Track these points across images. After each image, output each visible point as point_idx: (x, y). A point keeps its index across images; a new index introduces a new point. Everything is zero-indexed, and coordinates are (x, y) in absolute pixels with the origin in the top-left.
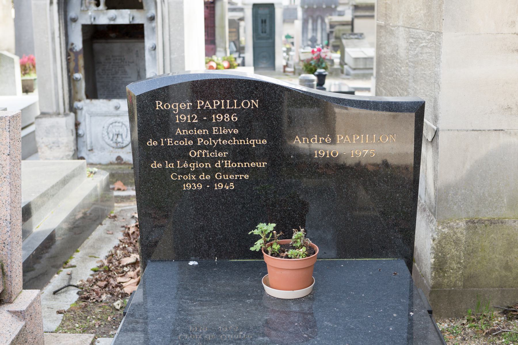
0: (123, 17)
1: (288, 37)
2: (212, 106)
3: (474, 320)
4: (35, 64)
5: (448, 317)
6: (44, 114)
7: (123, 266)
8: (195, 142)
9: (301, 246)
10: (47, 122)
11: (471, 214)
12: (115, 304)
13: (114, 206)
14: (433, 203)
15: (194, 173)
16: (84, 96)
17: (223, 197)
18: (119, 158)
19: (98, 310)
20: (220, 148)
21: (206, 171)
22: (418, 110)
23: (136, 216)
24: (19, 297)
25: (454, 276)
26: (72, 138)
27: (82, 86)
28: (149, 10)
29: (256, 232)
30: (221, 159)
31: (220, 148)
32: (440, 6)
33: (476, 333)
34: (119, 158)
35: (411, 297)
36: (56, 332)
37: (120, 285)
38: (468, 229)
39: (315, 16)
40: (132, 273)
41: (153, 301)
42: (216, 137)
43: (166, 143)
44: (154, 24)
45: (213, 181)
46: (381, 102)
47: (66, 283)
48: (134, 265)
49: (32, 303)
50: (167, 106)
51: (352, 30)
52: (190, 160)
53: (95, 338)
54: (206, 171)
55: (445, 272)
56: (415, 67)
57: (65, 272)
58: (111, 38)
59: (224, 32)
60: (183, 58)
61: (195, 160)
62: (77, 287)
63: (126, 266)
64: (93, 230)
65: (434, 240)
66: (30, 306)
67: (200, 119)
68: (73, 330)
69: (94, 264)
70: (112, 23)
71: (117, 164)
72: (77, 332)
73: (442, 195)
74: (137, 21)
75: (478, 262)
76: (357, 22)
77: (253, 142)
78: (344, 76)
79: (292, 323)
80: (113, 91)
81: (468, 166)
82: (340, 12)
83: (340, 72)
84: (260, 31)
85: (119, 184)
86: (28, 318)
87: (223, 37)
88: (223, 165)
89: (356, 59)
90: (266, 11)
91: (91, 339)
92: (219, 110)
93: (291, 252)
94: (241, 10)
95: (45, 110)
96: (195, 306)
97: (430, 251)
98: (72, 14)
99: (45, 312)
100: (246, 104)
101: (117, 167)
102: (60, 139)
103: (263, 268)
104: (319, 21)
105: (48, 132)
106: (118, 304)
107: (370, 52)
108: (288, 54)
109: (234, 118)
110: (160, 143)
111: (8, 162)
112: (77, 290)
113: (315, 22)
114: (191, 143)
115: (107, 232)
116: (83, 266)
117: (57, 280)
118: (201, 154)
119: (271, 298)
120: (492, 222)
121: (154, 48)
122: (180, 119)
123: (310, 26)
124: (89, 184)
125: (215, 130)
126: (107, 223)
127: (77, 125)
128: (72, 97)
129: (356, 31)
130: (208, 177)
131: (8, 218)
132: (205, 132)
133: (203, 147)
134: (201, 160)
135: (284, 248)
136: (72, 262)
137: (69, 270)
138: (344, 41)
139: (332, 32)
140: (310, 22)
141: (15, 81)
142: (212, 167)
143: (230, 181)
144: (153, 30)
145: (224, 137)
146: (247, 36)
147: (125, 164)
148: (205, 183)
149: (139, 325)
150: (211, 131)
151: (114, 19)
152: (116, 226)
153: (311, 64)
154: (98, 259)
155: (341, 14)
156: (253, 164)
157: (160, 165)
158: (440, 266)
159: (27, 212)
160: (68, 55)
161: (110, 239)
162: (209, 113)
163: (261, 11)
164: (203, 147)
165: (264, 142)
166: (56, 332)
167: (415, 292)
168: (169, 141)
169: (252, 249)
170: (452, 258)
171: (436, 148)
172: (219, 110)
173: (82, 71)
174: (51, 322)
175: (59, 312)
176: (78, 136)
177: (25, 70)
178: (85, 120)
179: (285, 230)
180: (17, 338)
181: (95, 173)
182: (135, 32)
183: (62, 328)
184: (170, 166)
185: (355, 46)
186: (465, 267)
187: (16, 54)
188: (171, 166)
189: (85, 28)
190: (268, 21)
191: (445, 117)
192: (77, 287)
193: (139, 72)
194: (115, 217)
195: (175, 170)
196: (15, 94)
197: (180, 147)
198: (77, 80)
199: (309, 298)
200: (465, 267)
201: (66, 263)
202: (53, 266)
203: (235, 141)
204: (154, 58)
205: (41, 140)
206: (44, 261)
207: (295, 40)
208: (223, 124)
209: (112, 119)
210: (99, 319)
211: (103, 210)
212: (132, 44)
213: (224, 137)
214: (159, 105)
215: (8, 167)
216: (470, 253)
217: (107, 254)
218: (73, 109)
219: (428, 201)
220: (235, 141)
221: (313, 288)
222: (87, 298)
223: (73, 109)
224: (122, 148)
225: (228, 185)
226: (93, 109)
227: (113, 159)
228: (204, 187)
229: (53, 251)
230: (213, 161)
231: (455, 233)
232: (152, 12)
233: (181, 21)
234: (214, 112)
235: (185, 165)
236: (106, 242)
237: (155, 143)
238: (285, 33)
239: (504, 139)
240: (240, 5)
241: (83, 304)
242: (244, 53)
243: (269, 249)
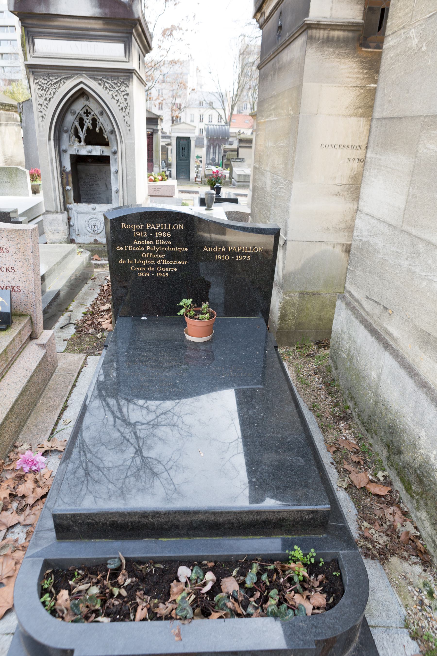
0: (96, 151)
1: (198, 157)
2: (156, 227)
3: (300, 348)
4: (40, 174)
5: (286, 346)
6: (48, 212)
7: (101, 312)
8: (145, 248)
9: (207, 313)
10: (50, 217)
11: (302, 289)
12: (98, 336)
13: (93, 272)
14: (282, 282)
15: (144, 267)
16: (73, 201)
17: (162, 281)
18: (95, 240)
19: (88, 339)
20: (160, 252)
21: (152, 266)
22: (276, 233)
23: (109, 278)
24: (42, 335)
25: (290, 323)
26: (67, 227)
27: (71, 194)
28: (113, 147)
29: (181, 304)
30: (161, 259)
31: (160, 252)
32: (293, 165)
33: (300, 355)
34: (95, 240)
35: (266, 342)
36: (63, 352)
37: (100, 324)
38: (300, 297)
39: (215, 144)
40: (106, 316)
41: (122, 342)
42: (158, 246)
43: (128, 248)
44: (116, 157)
45: (156, 271)
46: (255, 228)
47: (67, 322)
48: (108, 311)
49: (50, 339)
50: (129, 227)
51: (238, 156)
52: (142, 259)
53: (87, 356)
54: (152, 266)
55: (286, 321)
56: (275, 199)
57: (67, 314)
58: (88, 162)
59: (158, 154)
60: (135, 179)
61: (145, 259)
62: (74, 324)
63: (103, 311)
64: (82, 288)
65: (280, 303)
66: (48, 341)
67: (148, 234)
68: (73, 351)
69: (84, 310)
70: (89, 154)
71: (95, 244)
72: (76, 353)
73: (286, 278)
74: (106, 154)
75: (305, 316)
76: (240, 150)
77: (180, 249)
78: (231, 186)
79: (201, 357)
80: (91, 196)
81: (302, 262)
82: (230, 142)
83: (229, 184)
84: (181, 155)
85: (96, 257)
86: (48, 347)
87: (158, 157)
88: (162, 262)
89: (239, 175)
90: (185, 142)
91: (85, 357)
92: (160, 230)
93: (201, 316)
94: (169, 137)
95: (49, 209)
96: (146, 346)
97: (278, 309)
98: (63, 147)
99: (57, 340)
100: (176, 227)
101: (94, 245)
102: (59, 228)
103: (185, 325)
104: (217, 147)
105: (51, 224)
106: (99, 336)
107: (248, 171)
108: (197, 169)
109: (169, 235)
110: (124, 248)
111: (31, 257)
112: (75, 326)
113: (214, 147)
114: (143, 249)
115: (91, 288)
116: (77, 311)
117: (62, 320)
118: (149, 256)
119: (189, 341)
120: (313, 294)
121: (117, 172)
122: (136, 235)
123: (212, 150)
124: (79, 260)
125: (157, 241)
126: (90, 282)
127: (69, 219)
128: (66, 201)
129: (240, 157)
130: (153, 269)
131: (33, 290)
132: (151, 242)
133: (150, 252)
134: (149, 259)
135: (198, 313)
136: (71, 308)
137: (68, 314)
138: (232, 163)
139: (225, 155)
140: (212, 147)
141: (27, 186)
142: (155, 260)
143: (166, 272)
144: (116, 160)
145: (162, 246)
146: (173, 158)
147: (100, 244)
148: (151, 272)
149: (114, 357)
150: (155, 242)
151: (91, 152)
152: (96, 285)
153: (212, 180)
154: (86, 307)
155: (231, 144)
156: (179, 263)
157: (124, 262)
158: (283, 318)
159: (43, 278)
160: (62, 174)
161: (92, 293)
162: (154, 231)
163: (182, 142)
164: (150, 252)
165: (186, 249)
166: (63, 352)
167: (269, 339)
168: (130, 248)
169: (179, 314)
170: (290, 313)
171: (285, 250)
172: (160, 230)
173: (71, 185)
174: (61, 346)
175: (65, 340)
176: (70, 226)
177: (33, 178)
178: (74, 216)
179: (198, 303)
180: (42, 360)
181: (82, 252)
182: (104, 160)
183: (68, 350)
184: (131, 262)
185: (239, 167)
186: (297, 319)
187: (26, 168)
188: (131, 262)
189: (72, 156)
190: (186, 149)
191: (291, 235)
192: (74, 324)
193: (106, 185)
194: (95, 279)
195: (134, 264)
196: (28, 195)
197: (136, 251)
198: (68, 190)
199: (210, 342)
200: (297, 319)
201: (67, 309)
202: (60, 311)
203: (169, 249)
204: (117, 178)
205: (47, 228)
206: (53, 307)
207: (202, 159)
208: (162, 238)
209: (91, 216)
210: (88, 345)
211: (87, 274)
212: (102, 167)
213: (162, 246)
214: (124, 226)
215: (32, 260)
216: (300, 311)
217: (91, 303)
218: (66, 209)
219: (278, 280)
220: (169, 249)
221: (213, 336)
222: (81, 331)
223: (66, 209)
224: (98, 234)
225: (165, 274)
226: (79, 209)
227: (92, 241)
228: (151, 275)
229: (58, 301)
230: (156, 260)
231: (293, 300)
232: (115, 148)
233: (133, 155)
234: (157, 231)
235: (140, 262)
236: (89, 295)
237: (121, 249)
238: (196, 155)
239: (324, 247)
240: (168, 134)
241: (78, 335)
242: (171, 168)
243: (188, 314)
